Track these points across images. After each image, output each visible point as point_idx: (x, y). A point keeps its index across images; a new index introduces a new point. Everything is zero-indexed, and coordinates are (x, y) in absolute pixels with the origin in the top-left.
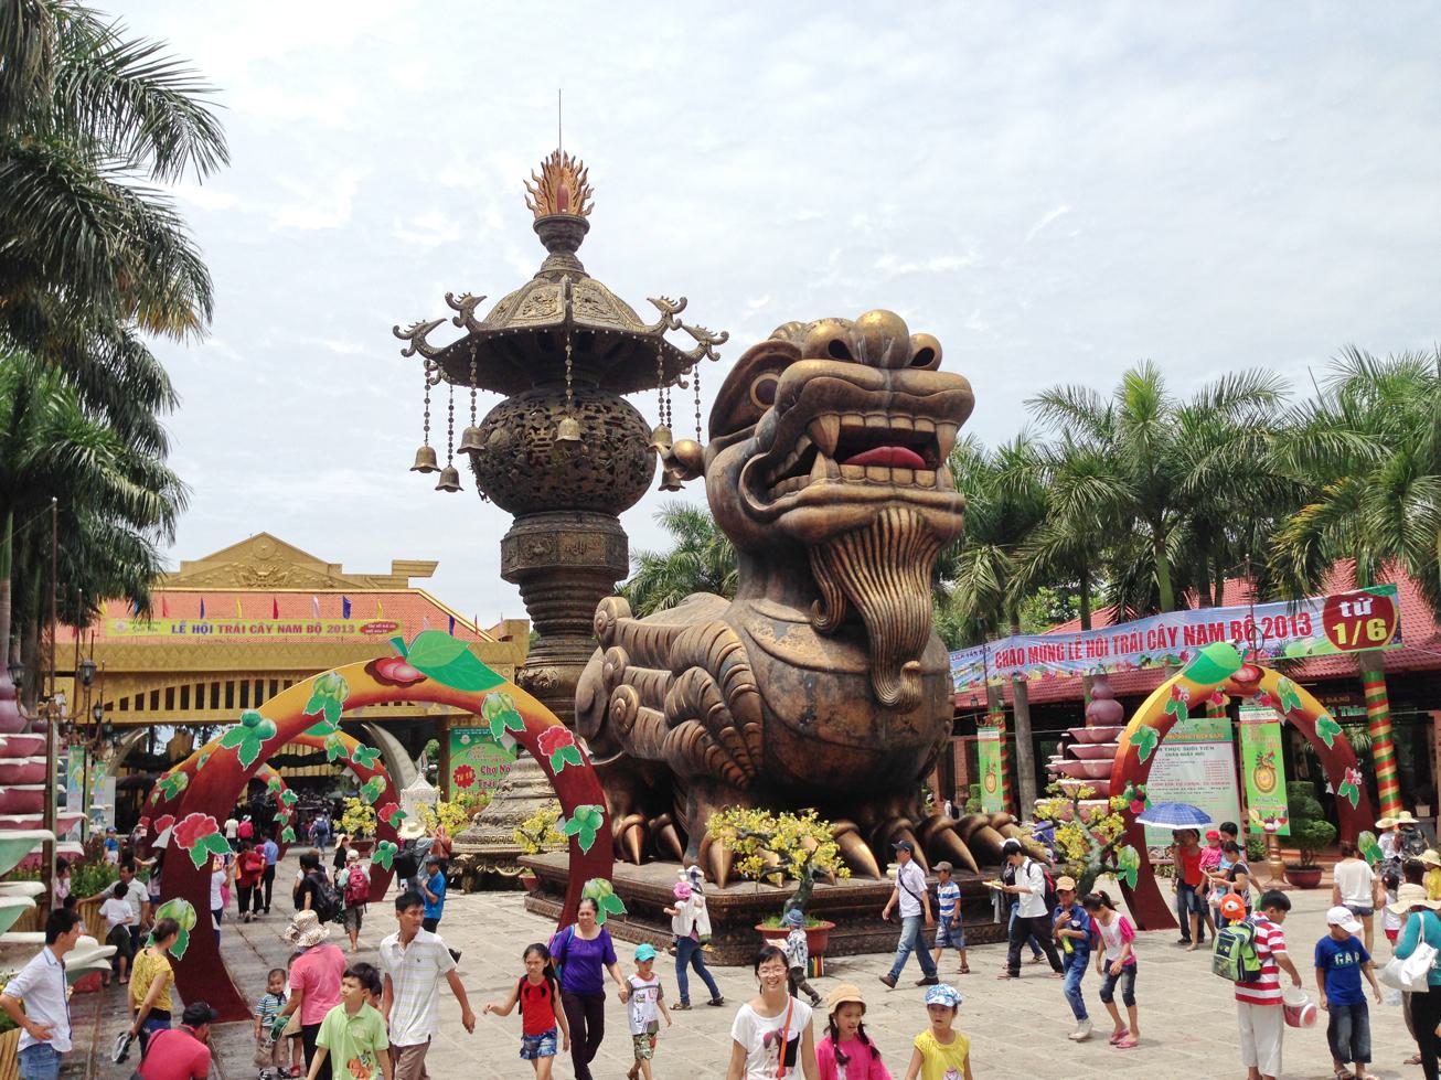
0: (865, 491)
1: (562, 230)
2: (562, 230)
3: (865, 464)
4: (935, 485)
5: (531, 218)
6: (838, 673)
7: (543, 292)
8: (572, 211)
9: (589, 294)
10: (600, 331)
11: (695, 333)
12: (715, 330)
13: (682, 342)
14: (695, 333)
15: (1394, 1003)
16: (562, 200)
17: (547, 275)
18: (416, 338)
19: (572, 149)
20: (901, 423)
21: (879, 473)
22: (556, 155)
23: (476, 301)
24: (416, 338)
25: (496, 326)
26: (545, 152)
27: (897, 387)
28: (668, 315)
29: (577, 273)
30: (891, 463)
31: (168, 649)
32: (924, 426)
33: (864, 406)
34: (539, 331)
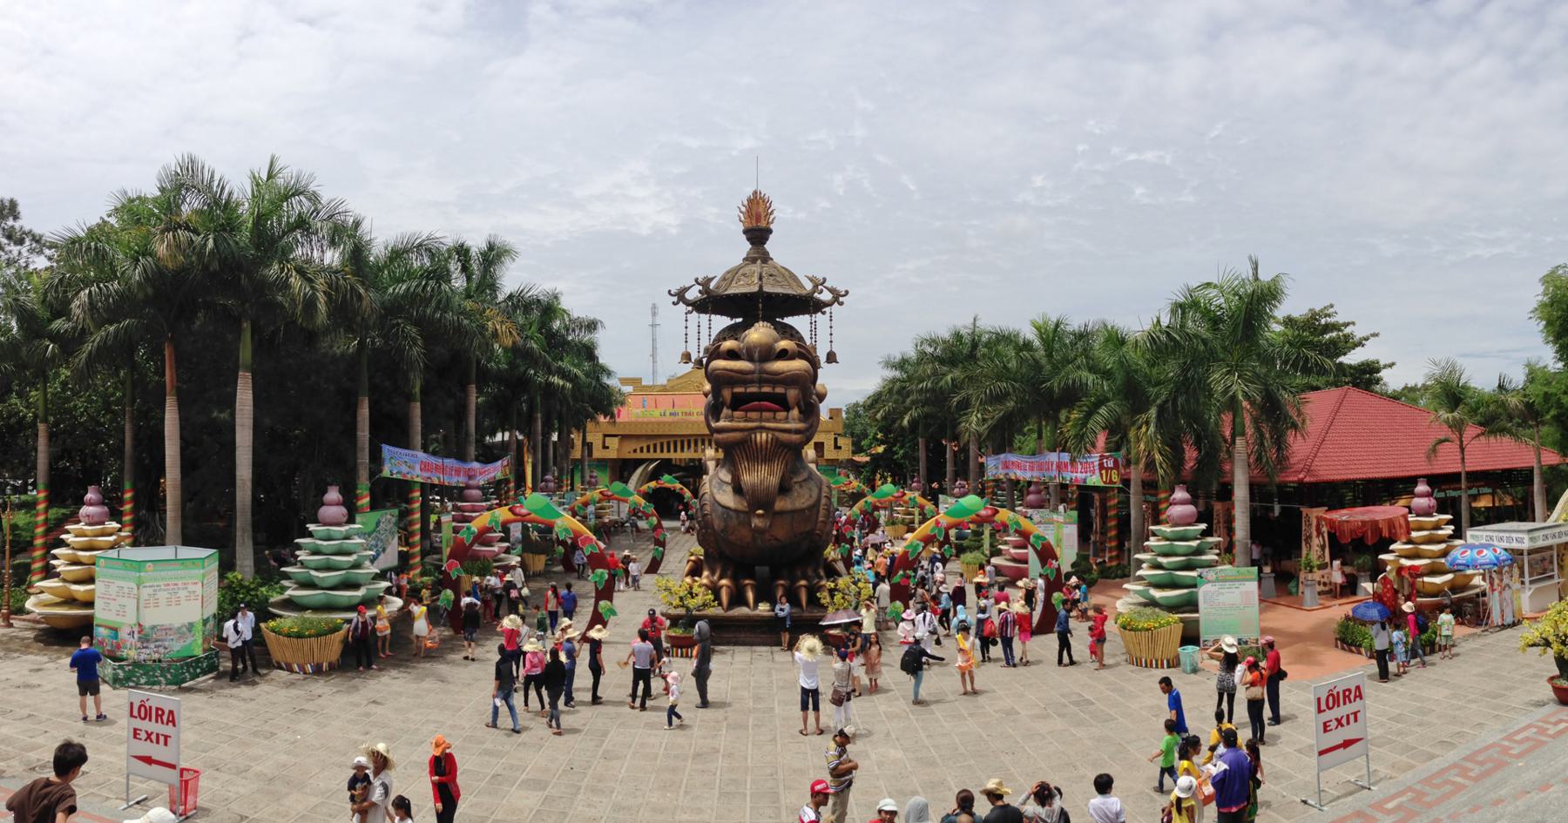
0: (742, 425)
1: (758, 235)
2: (758, 235)
3: (746, 411)
4: (786, 420)
5: (742, 228)
6: (736, 511)
7: (747, 270)
8: (763, 224)
9: (772, 271)
10: (777, 295)
11: (831, 290)
12: (842, 289)
13: (826, 296)
14: (831, 290)
15: (1268, 805)
16: (758, 219)
17: (750, 260)
18: (680, 296)
19: (766, 191)
20: (766, 389)
21: (754, 415)
22: (755, 193)
23: (687, 289)
24: (680, 296)
25: (720, 291)
26: (749, 192)
27: (763, 371)
28: (816, 286)
29: (765, 258)
30: (760, 410)
31: (659, 423)
32: (779, 390)
33: (745, 383)
34: (744, 295)
